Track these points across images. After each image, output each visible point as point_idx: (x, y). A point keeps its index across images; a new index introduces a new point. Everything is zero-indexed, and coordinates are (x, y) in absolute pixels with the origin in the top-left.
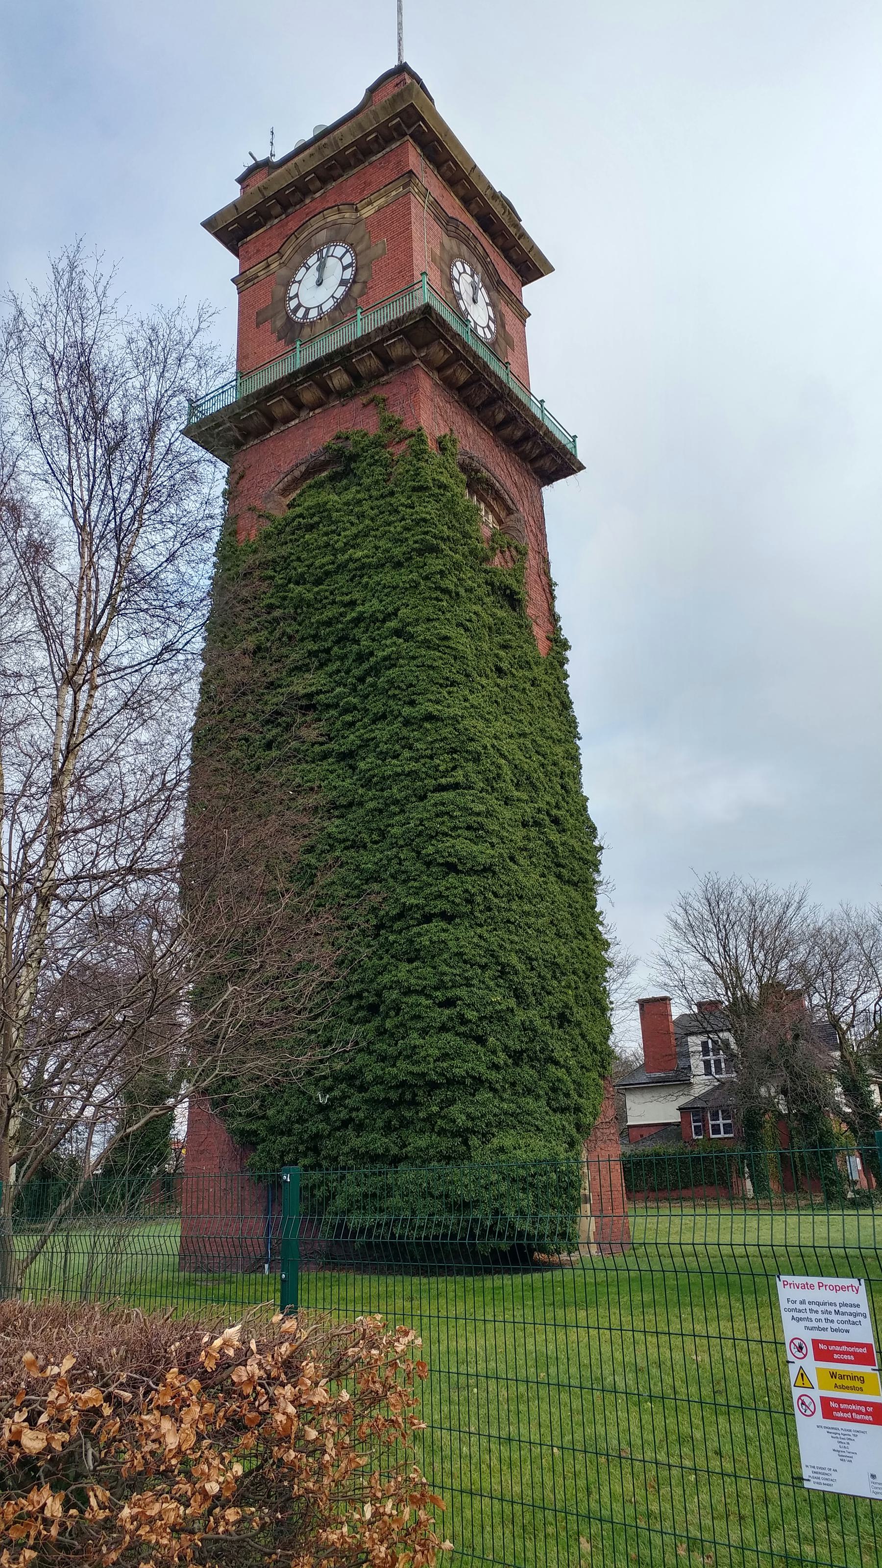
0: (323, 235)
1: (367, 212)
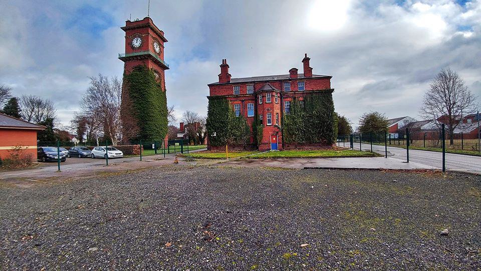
0: (137, 36)
1: (143, 35)
